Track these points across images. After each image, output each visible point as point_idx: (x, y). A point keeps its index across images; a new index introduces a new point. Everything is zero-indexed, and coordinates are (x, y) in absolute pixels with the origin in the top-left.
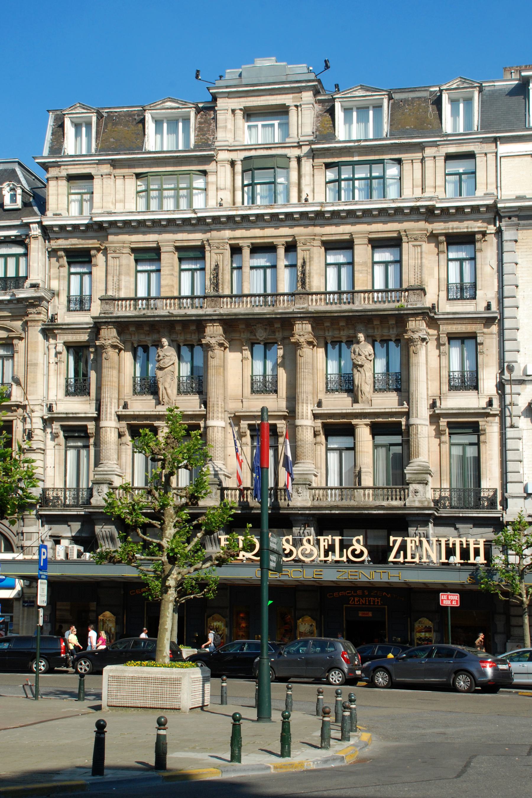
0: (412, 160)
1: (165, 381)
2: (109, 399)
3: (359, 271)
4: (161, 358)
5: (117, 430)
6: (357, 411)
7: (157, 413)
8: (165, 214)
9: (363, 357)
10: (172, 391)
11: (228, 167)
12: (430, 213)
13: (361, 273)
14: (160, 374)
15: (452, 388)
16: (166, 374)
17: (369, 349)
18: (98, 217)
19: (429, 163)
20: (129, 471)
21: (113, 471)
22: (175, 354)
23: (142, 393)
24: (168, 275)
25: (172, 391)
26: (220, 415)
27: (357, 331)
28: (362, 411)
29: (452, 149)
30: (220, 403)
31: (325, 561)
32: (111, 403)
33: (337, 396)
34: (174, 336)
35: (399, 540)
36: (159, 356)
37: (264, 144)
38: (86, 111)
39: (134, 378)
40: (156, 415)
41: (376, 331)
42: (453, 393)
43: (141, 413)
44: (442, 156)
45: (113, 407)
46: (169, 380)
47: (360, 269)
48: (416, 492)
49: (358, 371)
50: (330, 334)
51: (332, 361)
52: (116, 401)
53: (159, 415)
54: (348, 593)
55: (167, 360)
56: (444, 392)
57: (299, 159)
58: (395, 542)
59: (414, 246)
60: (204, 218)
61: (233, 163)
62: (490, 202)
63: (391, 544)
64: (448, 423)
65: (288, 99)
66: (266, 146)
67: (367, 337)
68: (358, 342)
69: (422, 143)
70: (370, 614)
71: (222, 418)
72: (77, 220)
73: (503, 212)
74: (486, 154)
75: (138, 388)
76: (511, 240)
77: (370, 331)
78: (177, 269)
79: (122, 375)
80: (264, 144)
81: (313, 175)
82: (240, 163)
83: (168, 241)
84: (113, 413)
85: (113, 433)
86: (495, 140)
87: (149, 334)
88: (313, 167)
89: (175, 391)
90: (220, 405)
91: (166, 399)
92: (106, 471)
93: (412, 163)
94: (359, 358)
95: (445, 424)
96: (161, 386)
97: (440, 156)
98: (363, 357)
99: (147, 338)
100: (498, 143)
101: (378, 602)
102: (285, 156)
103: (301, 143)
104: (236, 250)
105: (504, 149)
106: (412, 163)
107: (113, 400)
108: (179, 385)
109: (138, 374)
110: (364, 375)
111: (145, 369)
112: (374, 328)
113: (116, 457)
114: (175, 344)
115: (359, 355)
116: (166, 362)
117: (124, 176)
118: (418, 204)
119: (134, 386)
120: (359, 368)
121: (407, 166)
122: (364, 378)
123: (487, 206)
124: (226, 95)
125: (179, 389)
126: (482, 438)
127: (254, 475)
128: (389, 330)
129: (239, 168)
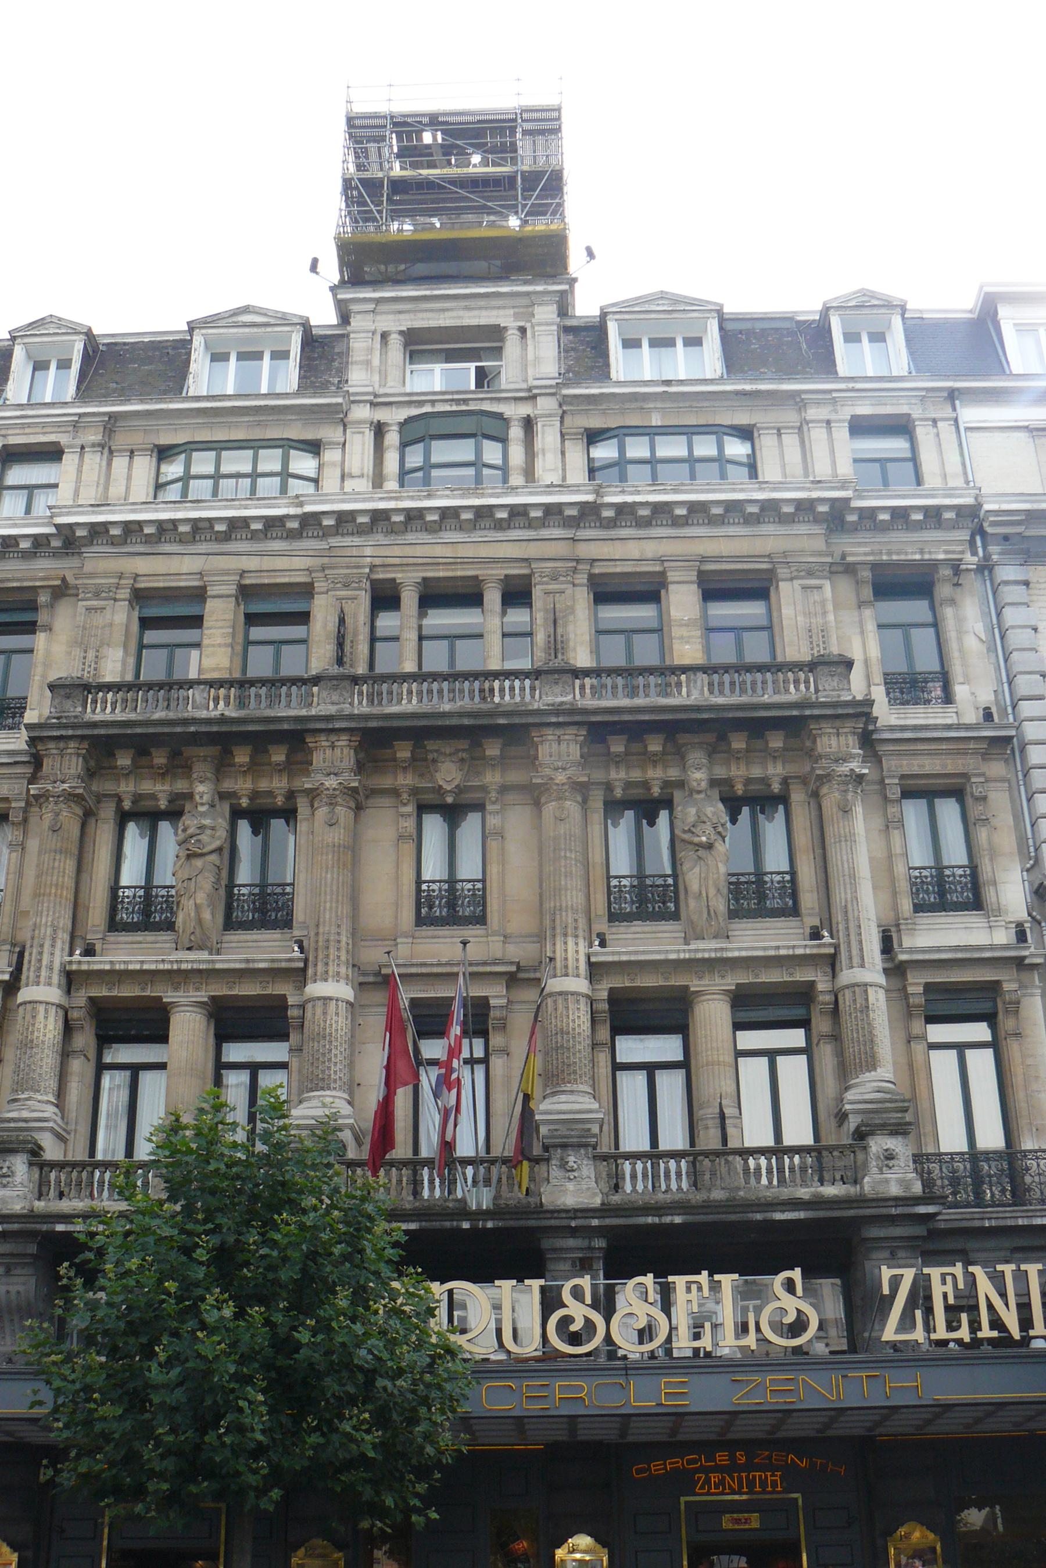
0: (779, 430)
2: (49, 931)
3: (682, 638)
5: (61, 1013)
8: (226, 508)
11: (369, 436)
12: (837, 518)
13: (687, 642)
15: (918, 908)
18: (68, 514)
19: (817, 435)
20: (84, 1129)
21: (45, 1120)
24: (220, 645)
26: (343, 970)
29: (864, 409)
30: (344, 939)
31: (696, 1351)
32: (54, 940)
33: (639, 929)
35: (909, 1275)
37: (452, 393)
42: (926, 919)
44: (843, 421)
45: (58, 952)
47: (685, 634)
48: (890, 1156)
52: (67, 937)
54: (689, 1462)
56: (907, 914)
57: (528, 424)
58: (895, 1282)
59: (805, 588)
60: (317, 516)
61: (379, 430)
62: (970, 501)
63: (886, 1291)
64: (928, 987)
65: (506, 316)
66: (456, 397)
69: (799, 392)
70: (755, 1521)
71: (347, 978)
72: (15, 526)
73: (994, 524)
74: (935, 421)
76: (1017, 583)
78: (240, 638)
79: (84, 876)
80: (452, 393)
81: (563, 453)
82: (396, 428)
83: (227, 572)
84: (57, 966)
85: (51, 1019)
86: (952, 396)
87: (163, 775)
88: (562, 435)
90: (343, 944)
92: (26, 1120)
93: (779, 435)
95: (921, 989)
97: (839, 421)
99: (159, 787)
100: (957, 402)
101: (774, 1484)
102: (499, 416)
103: (535, 391)
104: (385, 598)
105: (970, 414)
106: (779, 435)
107: (60, 934)
113: (53, 1084)
117: (132, 452)
118: (815, 495)
121: (767, 442)
123: (959, 509)
124: (371, 306)
126: (1007, 1024)
129: (392, 438)
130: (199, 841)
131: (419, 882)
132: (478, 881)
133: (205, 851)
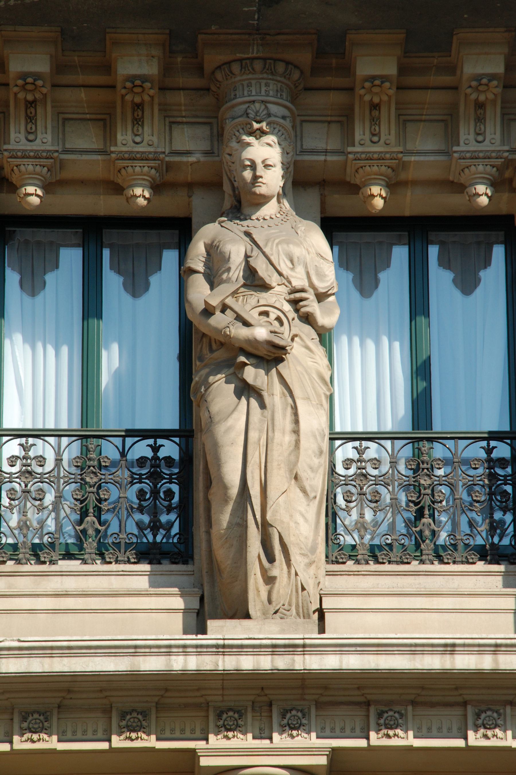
6: (247, 663)
9: (277, 297)
17: (306, 253)
25: (299, 520)
27: (222, 133)
28: (282, 663)
41: (361, 133)
49: (245, 390)
50: (45, 140)
51: (31, 340)
67: (300, 181)
68: (240, 203)
77: (320, 140)
94: (249, 304)
98: (277, 297)
110: (283, 421)
112: (345, 120)
115: (254, 281)
120: (252, 374)
122: (283, 439)
127: (203, 390)
128: (452, 136)
132: (166, 434)
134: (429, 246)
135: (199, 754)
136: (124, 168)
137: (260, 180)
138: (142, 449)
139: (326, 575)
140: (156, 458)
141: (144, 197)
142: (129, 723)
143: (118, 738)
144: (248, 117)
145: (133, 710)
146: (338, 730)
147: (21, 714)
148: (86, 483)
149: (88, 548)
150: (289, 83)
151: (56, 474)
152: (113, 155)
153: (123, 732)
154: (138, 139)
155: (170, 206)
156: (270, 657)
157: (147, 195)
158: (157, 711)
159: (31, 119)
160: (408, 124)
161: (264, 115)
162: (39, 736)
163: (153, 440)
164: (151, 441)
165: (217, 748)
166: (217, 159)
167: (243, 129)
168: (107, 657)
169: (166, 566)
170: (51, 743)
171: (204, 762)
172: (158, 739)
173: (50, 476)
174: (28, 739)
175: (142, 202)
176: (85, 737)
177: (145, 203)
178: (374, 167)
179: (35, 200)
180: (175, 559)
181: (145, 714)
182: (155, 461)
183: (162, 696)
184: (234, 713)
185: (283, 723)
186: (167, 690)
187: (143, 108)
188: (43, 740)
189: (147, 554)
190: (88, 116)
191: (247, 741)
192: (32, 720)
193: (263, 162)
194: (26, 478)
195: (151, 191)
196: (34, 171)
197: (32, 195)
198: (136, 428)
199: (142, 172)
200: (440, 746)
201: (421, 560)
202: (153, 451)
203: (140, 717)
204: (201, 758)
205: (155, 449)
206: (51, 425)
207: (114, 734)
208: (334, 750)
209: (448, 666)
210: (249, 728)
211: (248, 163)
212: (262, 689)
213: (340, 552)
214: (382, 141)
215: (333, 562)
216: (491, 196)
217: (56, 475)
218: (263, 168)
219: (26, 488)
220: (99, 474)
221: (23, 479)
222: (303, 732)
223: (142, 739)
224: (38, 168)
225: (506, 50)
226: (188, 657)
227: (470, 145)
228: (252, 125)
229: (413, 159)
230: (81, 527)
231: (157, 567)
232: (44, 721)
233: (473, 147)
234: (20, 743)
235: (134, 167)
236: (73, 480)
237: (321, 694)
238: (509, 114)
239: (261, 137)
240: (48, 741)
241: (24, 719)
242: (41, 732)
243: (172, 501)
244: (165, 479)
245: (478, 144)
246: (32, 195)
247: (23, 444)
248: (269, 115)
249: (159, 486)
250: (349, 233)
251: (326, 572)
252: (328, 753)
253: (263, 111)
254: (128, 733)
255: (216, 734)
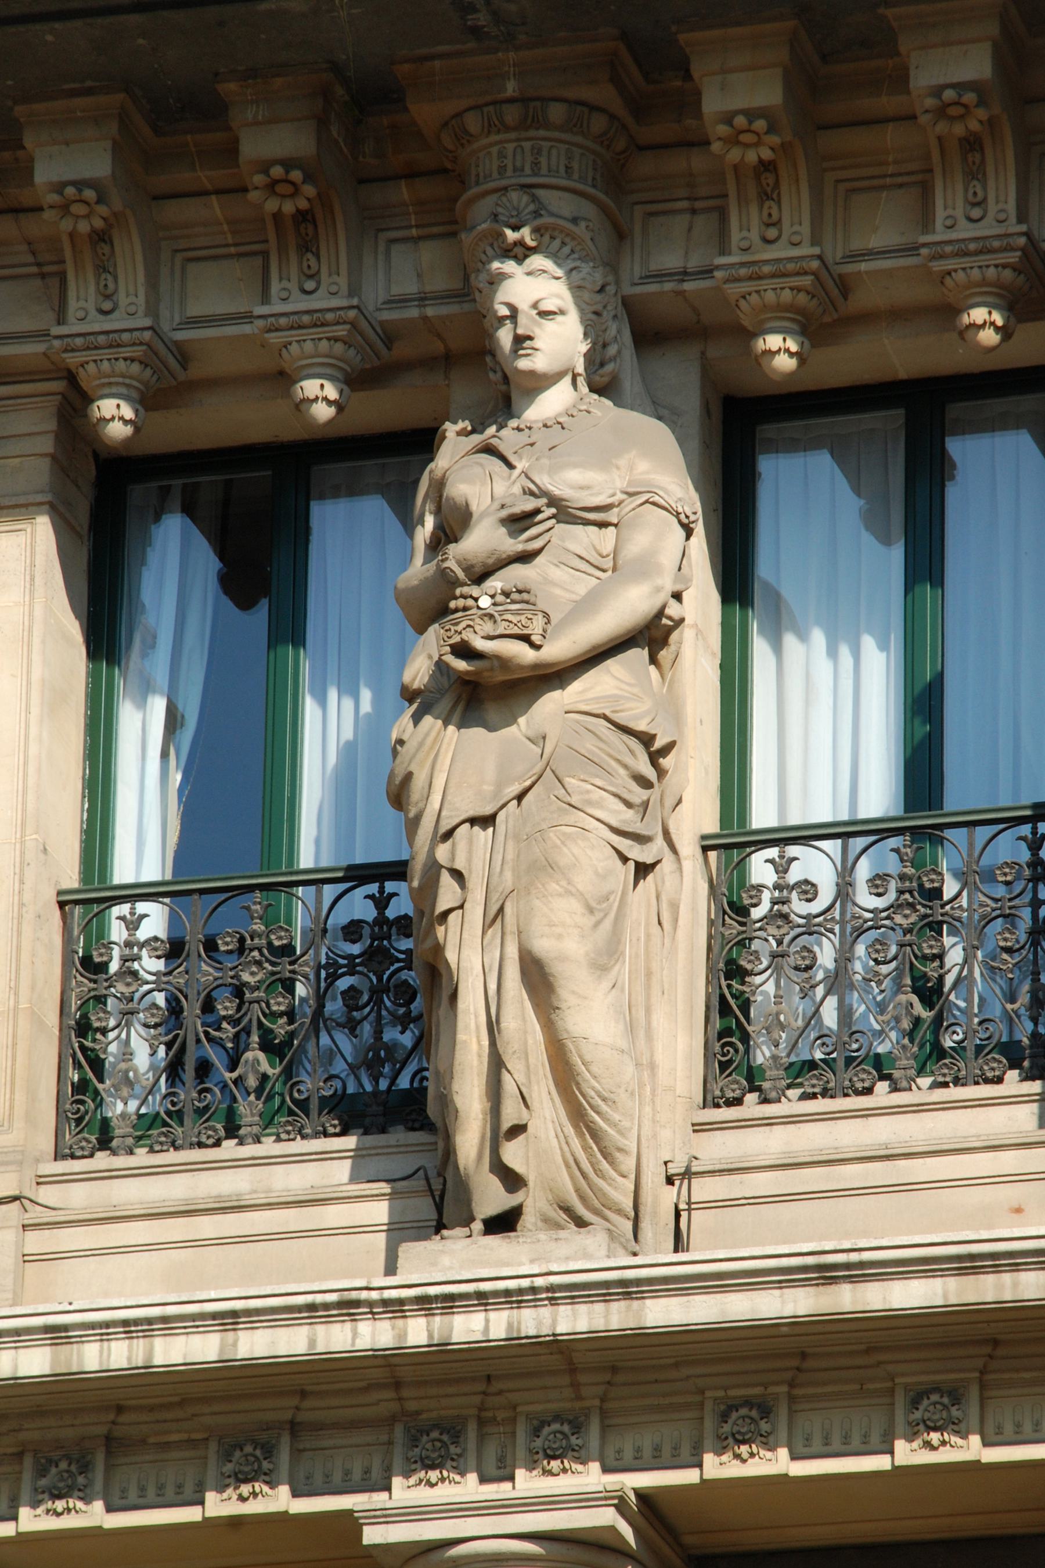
1: (541, 868)
4: (483, 539)
7: (418, 1332)
10: (635, 1024)
14: (459, 764)
16: (548, 772)
22: (682, 491)
23: (199, 1105)
25: (640, 1024)
34: (670, 252)
36: (453, 524)
38: (230, 894)
39: (90, 901)
40: (390, 1369)
43: (172, 1351)
46: (589, 858)
53: (444, 1362)
55: (559, 574)
75: (139, 1051)
89: (680, 1042)
91: (545, 1152)
96: (471, 956)
108: (729, 971)
109: (142, 851)
111: (235, 773)
114: (681, 374)
116: (571, 597)
119: (81, 1033)
125: (729, 1019)
130: (519, 595)
131: (733, 842)
133: (558, 649)
134: (312, 503)
135: (362, 1521)
136: (744, 297)
137: (528, 343)
138: (359, 905)
139: (694, 1131)
140: (381, 920)
141: (787, 350)
142: (927, 1415)
143: (32, 1512)
144: (497, 221)
145: (435, 1426)
146: (151, 1491)
147: (409, 1431)
148: (245, 984)
149: (771, 1069)
150: (589, 143)
151: (965, 904)
152: (718, 274)
153: (414, 1471)
154: (107, 306)
155: (387, 409)
156: (98, 1344)
157: (794, 347)
158: (109, 1453)
159: (103, 268)
160: (396, 248)
161: (528, 213)
162: (253, 1487)
163: (377, 884)
164: (373, 888)
165: (409, 1506)
166: (467, 307)
167: (492, 245)
168: (931, 1280)
169: (398, 1136)
170: (92, 1515)
171: (372, 1535)
172: (986, 1444)
173: (825, 920)
174: (421, 1481)
175: (989, 337)
176: (141, 1501)
177: (129, 430)
178: (117, 363)
179: (785, 363)
180: (414, 1121)
181: (453, 1430)
182: (381, 928)
183: (297, 1408)
184: (942, 1397)
185: (912, 1417)
186: (303, 1394)
187: (775, 169)
188: (450, 1482)
189: (350, 1114)
190: (233, 250)
191: (469, 1488)
192: (549, 1434)
193: (535, 306)
194: (779, 927)
195: (1006, 314)
196: (984, 279)
197: (982, 326)
198: (357, 862)
199: (303, 352)
200: (688, 1482)
201: (278, 1135)
202: (377, 908)
203: (445, 1438)
204: (365, 1528)
205: (381, 902)
206: (822, 813)
207: (397, 1475)
208: (643, 1496)
209: (599, 1324)
210: (472, 1461)
211: (504, 311)
212: (489, 1378)
213: (79, 1136)
214: (991, 214)
215: (64, 1157)
216: (1003, 327)
217: (838, 918)
218: (537, 317)
219: (780, 949)
220: (919, 907)
221: (772, 930)
222: (576, 1463)
223: (77, 1512)
224: (121, 365)
225: (993, 29)
226: (21, 1351)
227: (956, 227)
228: (503, 235)
229: (863, 266)
230: (234, 1075)
231: (371, 1140)
232: (261, 1458)
233: (965, 231)
234: (32, 1520)
235: (969, 271)
236: (998, 912)
237: (609, 1383)
238: (388, 229)
239: (526, 257)
240: (459, 1483)
241: (227, 1457)
242: (71, 1497)
243: (412, 1007)
244: (399, 960)
245: (976, 225)
246: (982, 326)
247: (125, 916)
248: (537, 214)
249: (385, 977)
250: (812, 421)
251: (693, 1125)
252: (616, 1502)
253: (527, 205)
254: (423, 1472)
255: (719, 1453)
